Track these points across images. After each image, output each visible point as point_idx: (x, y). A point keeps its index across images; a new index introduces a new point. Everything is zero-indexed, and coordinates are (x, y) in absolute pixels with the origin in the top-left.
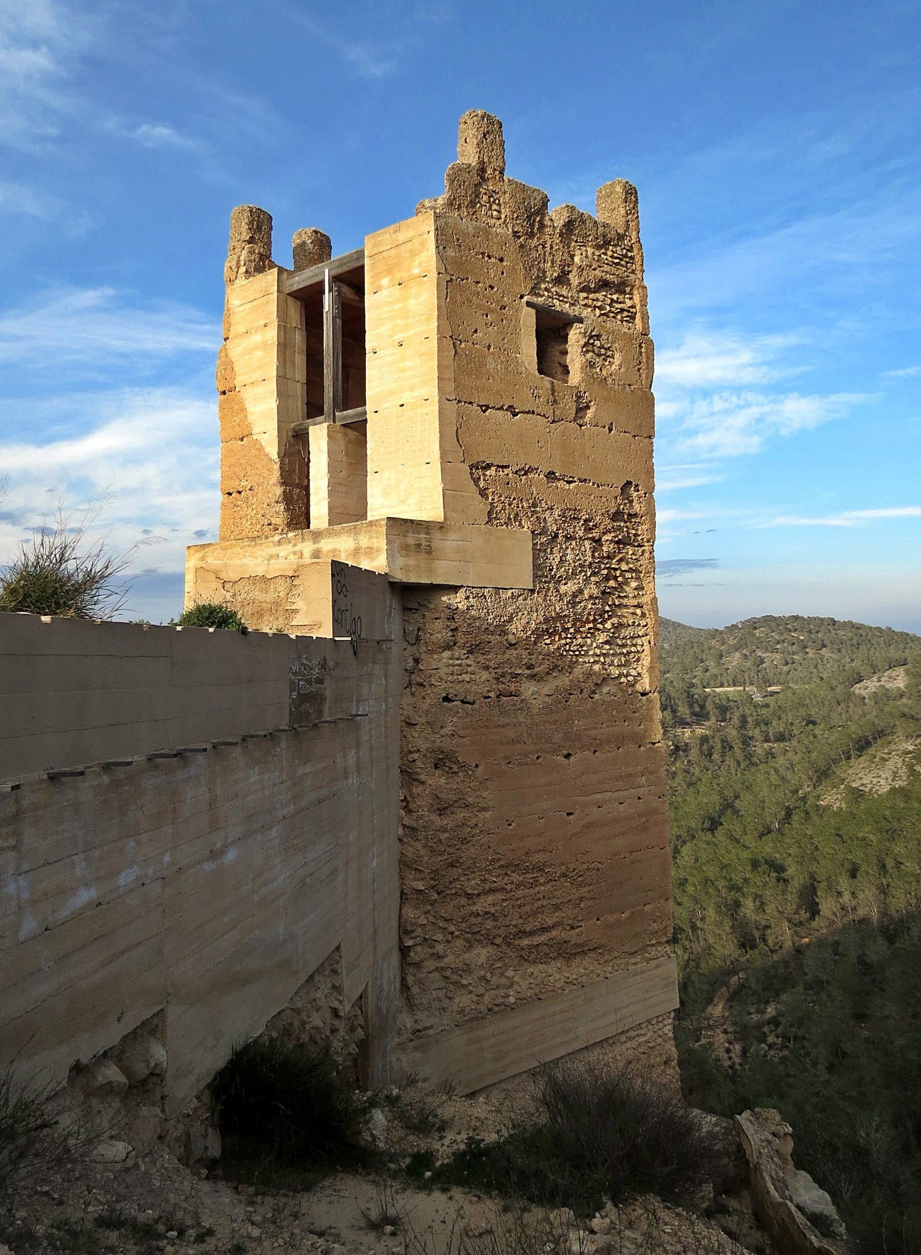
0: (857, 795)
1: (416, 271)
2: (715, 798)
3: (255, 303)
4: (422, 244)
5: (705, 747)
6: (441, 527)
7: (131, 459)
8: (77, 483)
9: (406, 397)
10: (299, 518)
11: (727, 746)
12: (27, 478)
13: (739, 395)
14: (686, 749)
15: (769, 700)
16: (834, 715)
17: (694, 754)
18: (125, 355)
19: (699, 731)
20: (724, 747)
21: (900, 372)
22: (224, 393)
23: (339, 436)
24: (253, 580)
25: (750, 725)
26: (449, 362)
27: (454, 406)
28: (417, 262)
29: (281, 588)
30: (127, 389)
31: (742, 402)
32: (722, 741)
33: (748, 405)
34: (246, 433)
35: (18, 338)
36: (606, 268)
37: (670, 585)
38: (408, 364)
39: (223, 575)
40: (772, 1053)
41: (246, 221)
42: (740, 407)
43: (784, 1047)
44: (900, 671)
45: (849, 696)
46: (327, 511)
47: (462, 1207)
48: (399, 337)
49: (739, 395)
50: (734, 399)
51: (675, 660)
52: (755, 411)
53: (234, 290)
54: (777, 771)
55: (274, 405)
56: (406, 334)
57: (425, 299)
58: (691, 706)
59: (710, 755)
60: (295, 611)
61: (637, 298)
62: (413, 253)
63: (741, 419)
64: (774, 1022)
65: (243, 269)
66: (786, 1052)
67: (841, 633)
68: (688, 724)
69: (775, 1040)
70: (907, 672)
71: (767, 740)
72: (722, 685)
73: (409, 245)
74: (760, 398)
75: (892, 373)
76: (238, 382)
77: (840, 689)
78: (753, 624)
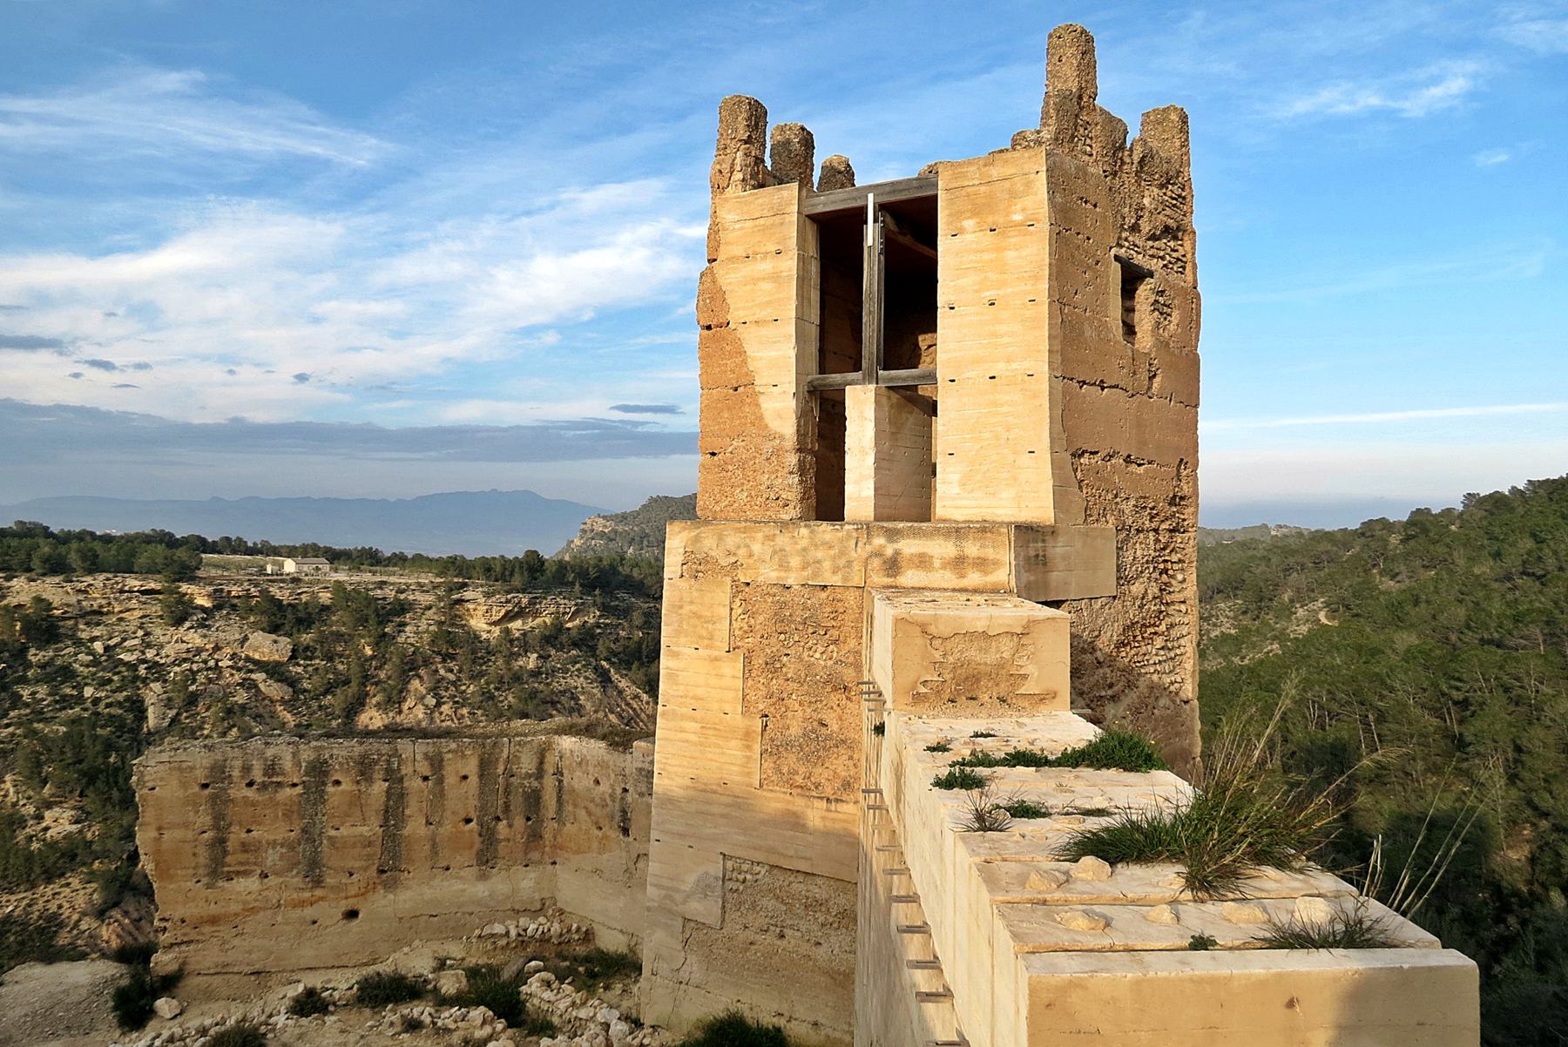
1: (1018, 217)
3: (762, 221)
4: (1028, 185)
6: (1053, 531)
7: (213, 281)
8: (141, 310)
9: (999, 368)
10: (826, 500)
12: (71, 297)
18: (211, 154)
22: (709, 328)
23: (884, 400)
24: (971, 636)
26: (1058, 331)
27: (1059, 384)
28: (1019, 207)
29: (1006, 648)
30: (212, 197)
34: (744, 381)
35: (72, 122)
36: (1168, 212)
38: (1003, 328)
39: (932, 630)
41: (745, 115)
46: (872, 493)
48: (989, 294)
53: (726, 200)
55: (793, 354)
56: (1001, 292)
57: (1031, 254)
60: (1025, 677)
61: (1188, 245)
62: (1013, 195)
65: (738, 176)
73: (1007, 184)
76: (735, 316)
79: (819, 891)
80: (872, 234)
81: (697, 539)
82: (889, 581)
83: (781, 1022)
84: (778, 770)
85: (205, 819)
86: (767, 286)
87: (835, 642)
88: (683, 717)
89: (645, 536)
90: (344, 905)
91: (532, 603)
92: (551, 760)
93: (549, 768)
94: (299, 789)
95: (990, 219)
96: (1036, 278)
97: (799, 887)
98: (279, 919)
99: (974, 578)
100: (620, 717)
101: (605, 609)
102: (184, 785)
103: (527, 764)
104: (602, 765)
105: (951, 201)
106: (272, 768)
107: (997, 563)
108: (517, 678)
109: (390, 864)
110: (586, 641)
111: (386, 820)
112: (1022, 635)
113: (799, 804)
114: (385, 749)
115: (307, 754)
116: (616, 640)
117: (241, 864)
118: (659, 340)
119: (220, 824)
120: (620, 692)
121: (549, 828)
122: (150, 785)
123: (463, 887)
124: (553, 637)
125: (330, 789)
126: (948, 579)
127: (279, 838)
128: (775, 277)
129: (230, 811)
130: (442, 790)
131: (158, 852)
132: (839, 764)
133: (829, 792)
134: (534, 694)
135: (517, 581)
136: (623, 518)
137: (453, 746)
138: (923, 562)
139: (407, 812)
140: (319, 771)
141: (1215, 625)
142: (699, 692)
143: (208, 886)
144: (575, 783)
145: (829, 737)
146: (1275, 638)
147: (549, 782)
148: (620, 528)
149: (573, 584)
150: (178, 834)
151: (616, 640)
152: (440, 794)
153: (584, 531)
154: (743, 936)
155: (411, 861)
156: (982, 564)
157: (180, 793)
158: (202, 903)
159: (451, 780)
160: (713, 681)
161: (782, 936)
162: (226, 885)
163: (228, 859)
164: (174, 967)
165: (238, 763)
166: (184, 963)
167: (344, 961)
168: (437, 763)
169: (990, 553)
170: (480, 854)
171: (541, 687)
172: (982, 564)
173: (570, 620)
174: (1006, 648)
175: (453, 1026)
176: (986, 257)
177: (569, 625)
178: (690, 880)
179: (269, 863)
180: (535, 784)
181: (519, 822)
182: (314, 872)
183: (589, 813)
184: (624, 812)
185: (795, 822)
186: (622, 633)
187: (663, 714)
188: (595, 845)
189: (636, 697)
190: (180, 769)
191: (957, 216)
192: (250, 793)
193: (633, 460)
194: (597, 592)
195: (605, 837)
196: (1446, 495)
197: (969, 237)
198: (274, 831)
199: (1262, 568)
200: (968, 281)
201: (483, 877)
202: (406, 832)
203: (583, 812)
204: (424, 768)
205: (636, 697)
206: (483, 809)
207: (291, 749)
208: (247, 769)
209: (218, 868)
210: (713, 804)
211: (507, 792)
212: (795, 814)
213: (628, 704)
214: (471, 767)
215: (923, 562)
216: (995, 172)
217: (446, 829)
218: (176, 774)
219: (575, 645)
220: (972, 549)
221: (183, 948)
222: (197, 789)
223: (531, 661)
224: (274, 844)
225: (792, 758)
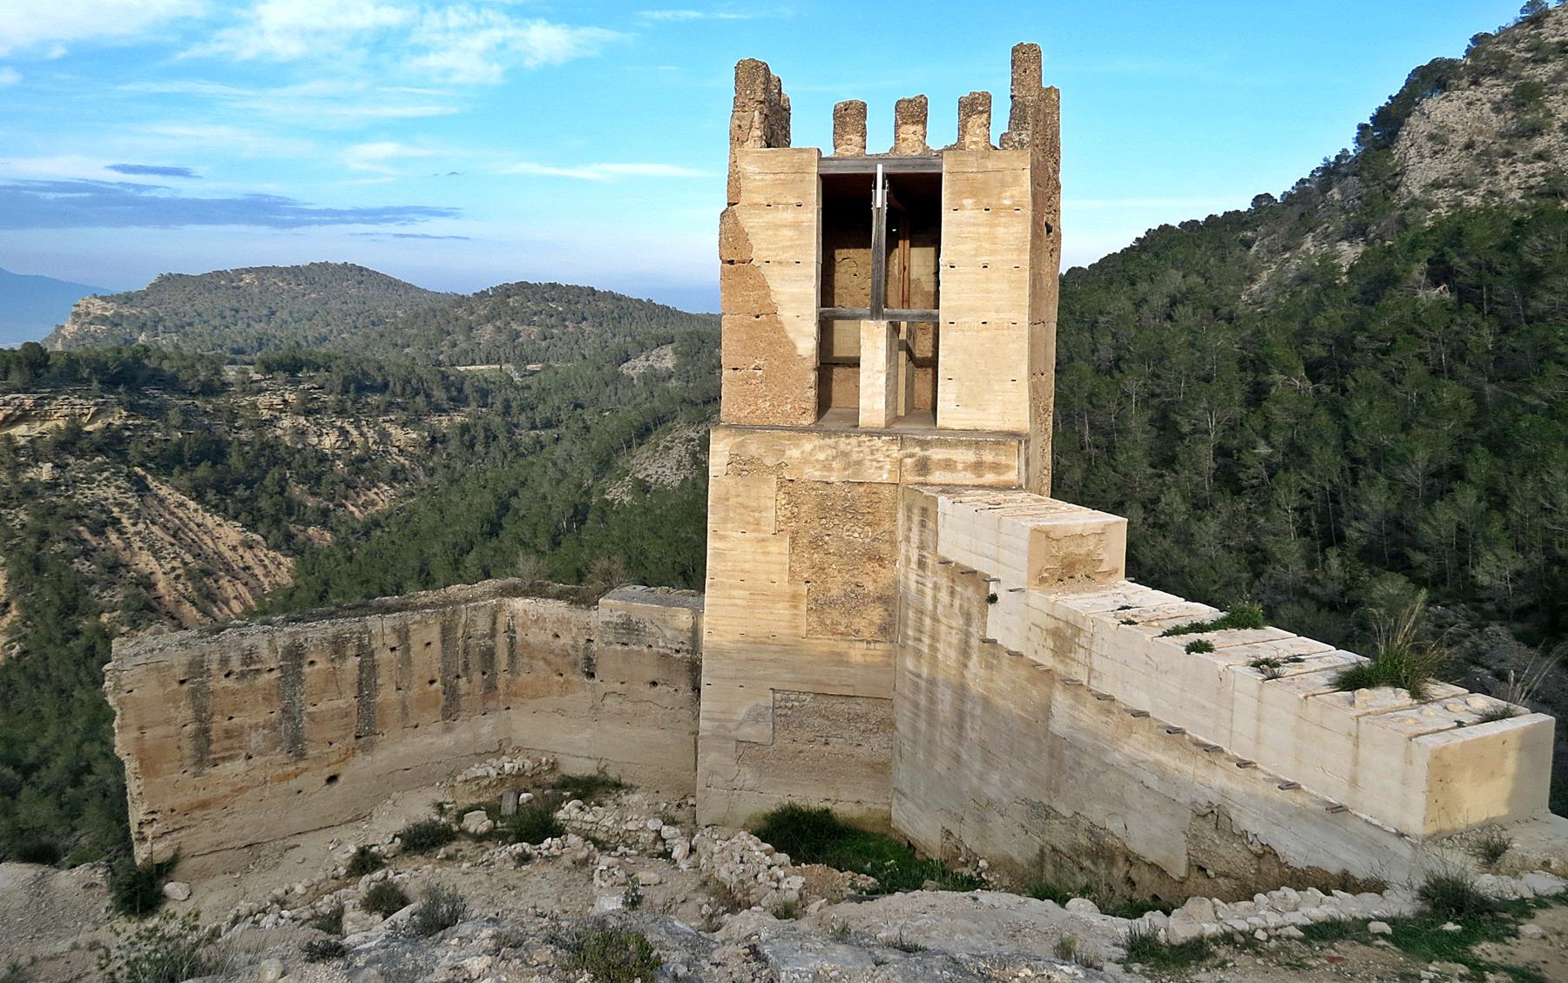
0: (642, 487)
1: (1007, 202)
2: (488, 496)
4: (1016, 179)
5: (466, 437)
9: (990, 317)
11: (491, 437)
13: (478, 12)
14: (444, 439)
15: (529, 380)
16: (602, 398)
17: (453, 446)
19: (458, 419)
20: (487, 437)
21: (657, 15)
22: (731, 262)
25: (515, 410)
31: (482, 21)
32: (486, 430)
33: (489, 25)
37: (402, 236)
38: (994, 286)
42: (479, 27)
44: (668, 349)
45: (619, 375)
48: (984, 259)
49: (478, 12)
50: (473, 16)
51: (415, 331)
52: (497, 34)
53: (747, 153)
54: (555, 464)
58: (448, 389)
59: (472, 446)
62: (1004, 184)
63: (481, 41)
67: (601, 304)
68: (445, 411)
70: (675, 352)
71: (534, 428)
72: (473, 363)
73: (999, 175)
74: (504, 19)
75: (647, 13)
76: (759, 254)
77: (607, 368)
78: (506, 291)
79: (860, 707)
80: (880, 198)
81: (742, 445)
82: (921, 479)
83: (829, 805)
84: (822, 623)
85: (186, 713)
86: (788, 233)
87: (869, 525)
88: (732, 587)
89: (158, 321)
90: (327, 773)
91: (36, 405)
92: (503, 620)
93: (501, 627)
94: (276, 674)
95: (985, 201)
96: (1020, 251)
97: (840, 706)
98: (267, 794)
99: (990, 478)
100: (165, 527)
101: (133, 409)
102: (163, 685)
103: (483, 625)
104: (562, 621)
105: (953, 183)
106: (249, 657)
107: (1008, 467)
108: (29, 492)
109: (366, 727)
110: (112, 444)
111: (361, 691)
112: (1101, 534)
113: (842, 646)
114: (357, 627)
115: (282, 640)
116: (152, 442)
117: (227, 750)
118: (156, 88)
120: (162, 501)
121: (502, 679)
122: (128, 688)
123: (434, 740)
124: (70, 442)
125: (307, 669)
126: (969, 478)
127: (261, 721)
128: (796, 226)
129: (210, 702)
130: (409, 659)
131: (141, 751)
133: (867, 635)
134: (52, 510)
135: (15, 378)
136: (128, 299)
137: (418, 617)
138: (949, 465)
139: (379, 681)
140: (295, 654)
142: (747, 566)
143: (195, 775)
144: (530, 639)
145: (867, 595)
147: (502, 640)
148: (125, 311)
149: (88, 381)
150: (160, 731)
151: (152, 442)
152: (407, 661)
153: (77, 315)
154: (791, 747)
155: (384, 724)
157: (160, 692)
158: (190, 791)
159: (416, 647)
160: (763, 558)
161: (827, 743)
162: (213, 770)
163: (212, 747)
164: (169, 854)
165: (216, 657)
166: (179, 849)
167: (331, 822)
168: (403, 634)
169: (1003, 459)
170: (445, 709)
171: (61, 501)
172: (996, 467)
173: (90, 422)
174: (1091, 544)
175: (558, 853)
176: (982, 230)
177: (88, 428)
178: (742, 712)
179: (253, 745)
180: (489, 643)
181: (477, 677)
182: (296, 747)
183: (548, 663)
184: (589, 659)
185: (840, 660)
186: (157, 435)
187: (712, 585)
188: (556, 688)
189: (181, 505)
190: (158, 670)
192: (230, 683)
193: (134, 230)
194: (121, 389)
195: (567, 682)
197: (967, 213)
198: (255, 716)
200: (968, 247)
201: (448, 729)
202: (378, 700)
203: (541, 663)
204: (392, 641)
205: (181, 505)
206: (445, 670)
207: (267, 637)
208: (224, 661)
209: (204, 752)
210: (757, 650)
211: (466, 652)
212: (839, 654)
213: (172, 513)
214: (434, 634)
215: (949, 465)
216: (990, 165)
217: (415, 691)
218: (155, 674)
219: (99, 450)
220: (988, 457)
221: (175, 835)
222: (176, 686)
223: (45, 472)
224: (255, 727)
225: (835, 614)
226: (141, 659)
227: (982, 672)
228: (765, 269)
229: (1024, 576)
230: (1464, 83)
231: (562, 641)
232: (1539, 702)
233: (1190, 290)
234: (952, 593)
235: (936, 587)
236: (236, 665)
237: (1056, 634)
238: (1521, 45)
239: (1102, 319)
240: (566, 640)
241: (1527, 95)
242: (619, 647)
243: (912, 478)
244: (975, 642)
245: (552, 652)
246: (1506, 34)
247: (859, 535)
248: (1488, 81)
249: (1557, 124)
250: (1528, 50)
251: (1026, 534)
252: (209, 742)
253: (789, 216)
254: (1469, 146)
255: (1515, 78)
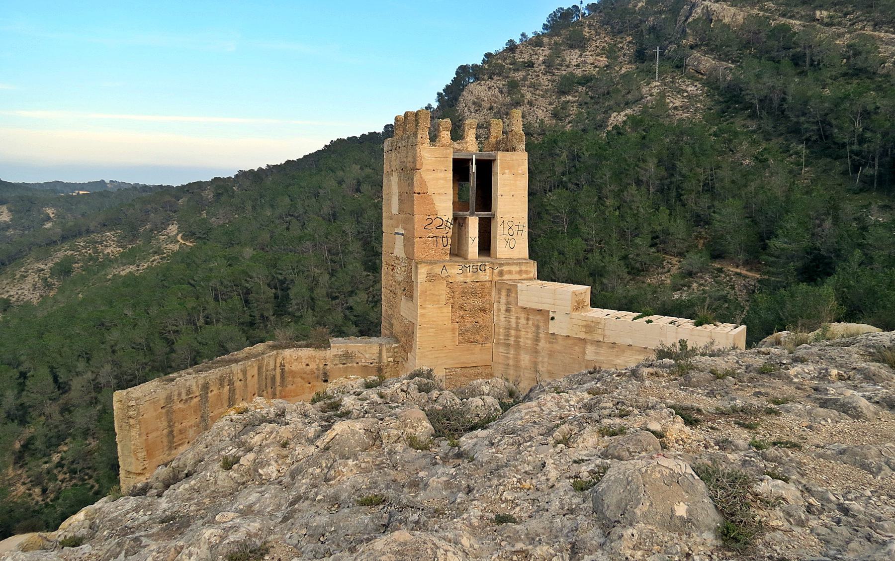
40: (64, 485)
43: (71, 479)
47: (591, 251)
48: (512, 193)
62: (519, 166)
64: (60, 465)
66: (74, 481)
69: (63, 476)
70: (10, 211)
81: (432, 269)
86: (442, 182)
93: (278, 365)
97: (471, 371)
99: (524, 276)
105: (501, 163)
107: (530, 272)
119: (171, 426)
121: (279, 389)
128: (445, 179)
132: (484, 333)
138: (510, 272)
140: (206, 387)
141: (106, 246)
144: (293, 368)
146: (155, 253)
152: (246, 386)
156: (527, 272)
165: (176, 393)
168: (244, 372)
169: (529, 269)
172: (527, 272)
191: (503, 168)
192: (181, 406)
196: (229, 170)
199: (131, 210)
204: (241, 377)
208: (180, 394)
214: (255, 371)
215: (510, 272)
224: (191, 427)
226: (147, 398)
227: (548, 345)
228: (433, 197)
229: (569, 308)
230: (486, 77)
231: (311, 367)
232: (743, 322)
233: (368, 176)
234: (528, 319)
235: (517, 318)
236: (184, 397)
237: (586, 326)
238: (507, 61)
239: (321, 191)
240: (313, 366)
241: (513, 86)
242: (341, 366)
243: (497, 278)
244: (542, 335)
245: (305, 373)
246: (499, 54)
247: (478, 302)
248: (495, 78)
249: (526, 101)
250: (510, 64)
251: (570, 294)
252: (174, 437)
253: (442, 175)
254: (491, 108)
255: (507, 77)
